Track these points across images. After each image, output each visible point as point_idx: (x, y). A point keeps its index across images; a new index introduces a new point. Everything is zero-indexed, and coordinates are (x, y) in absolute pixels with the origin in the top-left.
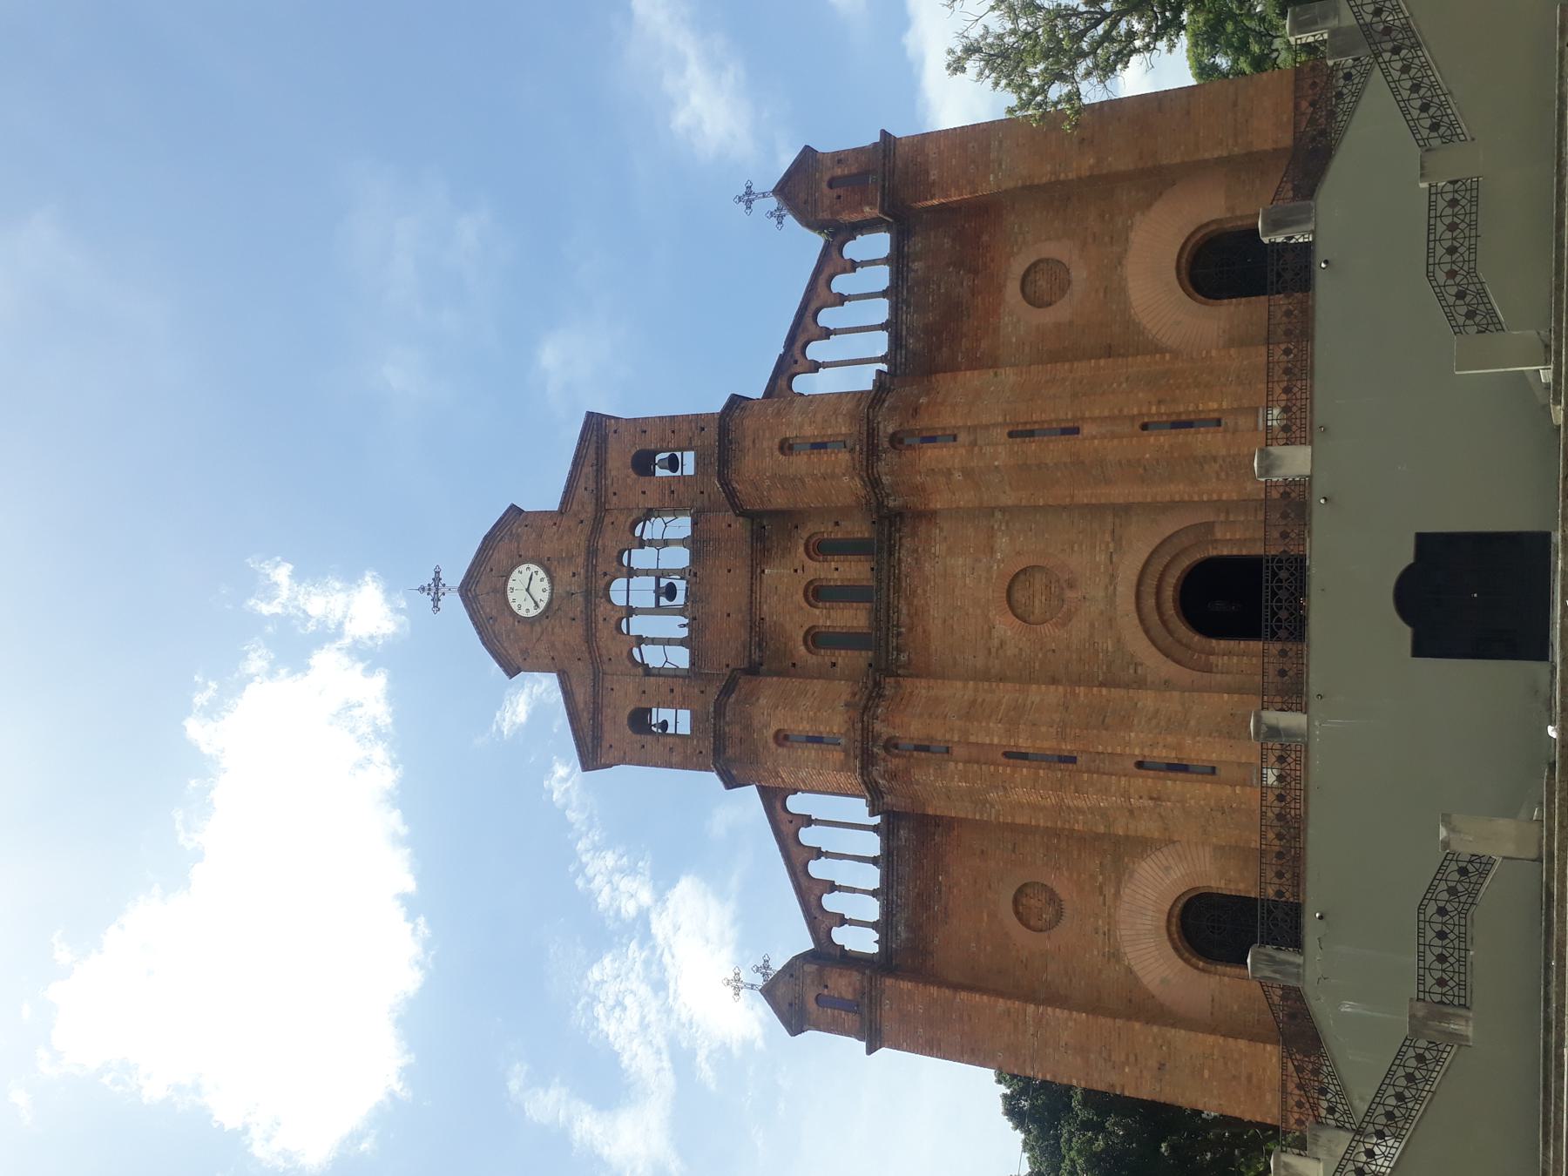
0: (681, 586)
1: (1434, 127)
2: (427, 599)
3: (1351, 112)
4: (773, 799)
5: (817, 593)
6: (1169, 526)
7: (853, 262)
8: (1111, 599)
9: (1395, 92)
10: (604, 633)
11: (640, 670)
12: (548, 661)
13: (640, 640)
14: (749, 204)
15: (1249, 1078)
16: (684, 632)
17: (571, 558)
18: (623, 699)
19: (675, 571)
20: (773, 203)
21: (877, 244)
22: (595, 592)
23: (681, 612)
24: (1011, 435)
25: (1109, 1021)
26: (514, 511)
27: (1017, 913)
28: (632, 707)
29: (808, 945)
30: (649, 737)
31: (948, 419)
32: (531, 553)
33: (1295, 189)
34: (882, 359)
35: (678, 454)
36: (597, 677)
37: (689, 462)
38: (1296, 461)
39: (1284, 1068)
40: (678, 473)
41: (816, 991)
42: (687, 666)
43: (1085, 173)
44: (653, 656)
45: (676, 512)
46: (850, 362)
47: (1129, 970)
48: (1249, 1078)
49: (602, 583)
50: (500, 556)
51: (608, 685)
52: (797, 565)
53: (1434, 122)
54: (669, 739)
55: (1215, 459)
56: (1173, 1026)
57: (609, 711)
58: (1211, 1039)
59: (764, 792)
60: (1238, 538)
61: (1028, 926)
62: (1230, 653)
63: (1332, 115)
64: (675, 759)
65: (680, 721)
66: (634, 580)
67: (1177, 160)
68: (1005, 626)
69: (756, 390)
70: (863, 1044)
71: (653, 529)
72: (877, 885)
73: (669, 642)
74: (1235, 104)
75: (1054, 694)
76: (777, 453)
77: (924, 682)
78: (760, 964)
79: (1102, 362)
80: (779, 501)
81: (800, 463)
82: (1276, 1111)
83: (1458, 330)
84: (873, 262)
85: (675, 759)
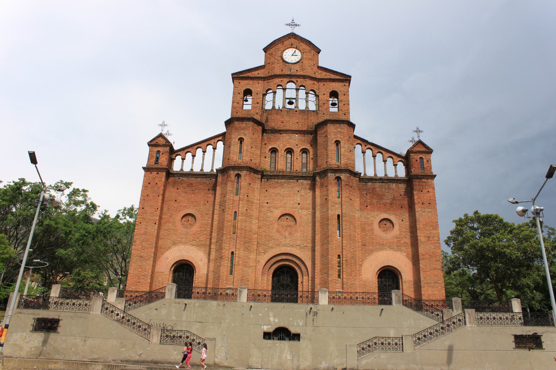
0: (292, 107)
1: (419, 339)
2: (290, 22)
3: (427, 316)
4: (223, 137)
6: (309, 264)
7: (397, 165)
8: (285, 245)
9: (430, 328)
10: (277, 81)
12: (268, 62)
13: (275, 93)
14: (416, 131)
15: (139, 282)
16: (277, 108)
17: (303, 70)
18: (257, 87)
19: (297, 104)
20: (417, 139)
21: (401, 172)
22: (291, 77)
23: (284, 107)
24: (338, 216)
25: (154, 242)
26: (318, 51)
28: (252, 90)
29: (176, 148)
30: (242, 96)
31: (345, 194)
32: (304, 56)
33: (406, 301)
34: (365, 174)
35: (337, 106)
37: (334, 110)
38: (323, 299)
39: (142, 292)
40: (330, 106)
41: (162, 149)
42: (266, 108)
43: (419, 238)
44: (269, 97)
45: (318, 105)
46: (368, 165)
47: (170, 248)
48: (139, 282)
49: (294, 80)
50: (303, 46)
51: (260, 81)
53: (421, 338)
54: (241, 102)
55: (328, 277)
58: (150, 271)
59: (224, 135)
60: (304, 283)
61: (183, 217)
62: (268, 280)
63: (427, 310)
64: (235, 104)
65: (248, 106)
66: (295, 91)
67: (421, 266)
68: (278, 213)
69: (357, 132)
70: (145, 166)
71: (312, 97)
72: (194, 171)
73: (274, 102)
74: (436, 283)
77: (259, 187)
78: (170, 133)
79: (360, 243)
80: (320, 140)
82: (130, 289)
83: (359, 345)
84: (396, 172)
85: (235, 104)
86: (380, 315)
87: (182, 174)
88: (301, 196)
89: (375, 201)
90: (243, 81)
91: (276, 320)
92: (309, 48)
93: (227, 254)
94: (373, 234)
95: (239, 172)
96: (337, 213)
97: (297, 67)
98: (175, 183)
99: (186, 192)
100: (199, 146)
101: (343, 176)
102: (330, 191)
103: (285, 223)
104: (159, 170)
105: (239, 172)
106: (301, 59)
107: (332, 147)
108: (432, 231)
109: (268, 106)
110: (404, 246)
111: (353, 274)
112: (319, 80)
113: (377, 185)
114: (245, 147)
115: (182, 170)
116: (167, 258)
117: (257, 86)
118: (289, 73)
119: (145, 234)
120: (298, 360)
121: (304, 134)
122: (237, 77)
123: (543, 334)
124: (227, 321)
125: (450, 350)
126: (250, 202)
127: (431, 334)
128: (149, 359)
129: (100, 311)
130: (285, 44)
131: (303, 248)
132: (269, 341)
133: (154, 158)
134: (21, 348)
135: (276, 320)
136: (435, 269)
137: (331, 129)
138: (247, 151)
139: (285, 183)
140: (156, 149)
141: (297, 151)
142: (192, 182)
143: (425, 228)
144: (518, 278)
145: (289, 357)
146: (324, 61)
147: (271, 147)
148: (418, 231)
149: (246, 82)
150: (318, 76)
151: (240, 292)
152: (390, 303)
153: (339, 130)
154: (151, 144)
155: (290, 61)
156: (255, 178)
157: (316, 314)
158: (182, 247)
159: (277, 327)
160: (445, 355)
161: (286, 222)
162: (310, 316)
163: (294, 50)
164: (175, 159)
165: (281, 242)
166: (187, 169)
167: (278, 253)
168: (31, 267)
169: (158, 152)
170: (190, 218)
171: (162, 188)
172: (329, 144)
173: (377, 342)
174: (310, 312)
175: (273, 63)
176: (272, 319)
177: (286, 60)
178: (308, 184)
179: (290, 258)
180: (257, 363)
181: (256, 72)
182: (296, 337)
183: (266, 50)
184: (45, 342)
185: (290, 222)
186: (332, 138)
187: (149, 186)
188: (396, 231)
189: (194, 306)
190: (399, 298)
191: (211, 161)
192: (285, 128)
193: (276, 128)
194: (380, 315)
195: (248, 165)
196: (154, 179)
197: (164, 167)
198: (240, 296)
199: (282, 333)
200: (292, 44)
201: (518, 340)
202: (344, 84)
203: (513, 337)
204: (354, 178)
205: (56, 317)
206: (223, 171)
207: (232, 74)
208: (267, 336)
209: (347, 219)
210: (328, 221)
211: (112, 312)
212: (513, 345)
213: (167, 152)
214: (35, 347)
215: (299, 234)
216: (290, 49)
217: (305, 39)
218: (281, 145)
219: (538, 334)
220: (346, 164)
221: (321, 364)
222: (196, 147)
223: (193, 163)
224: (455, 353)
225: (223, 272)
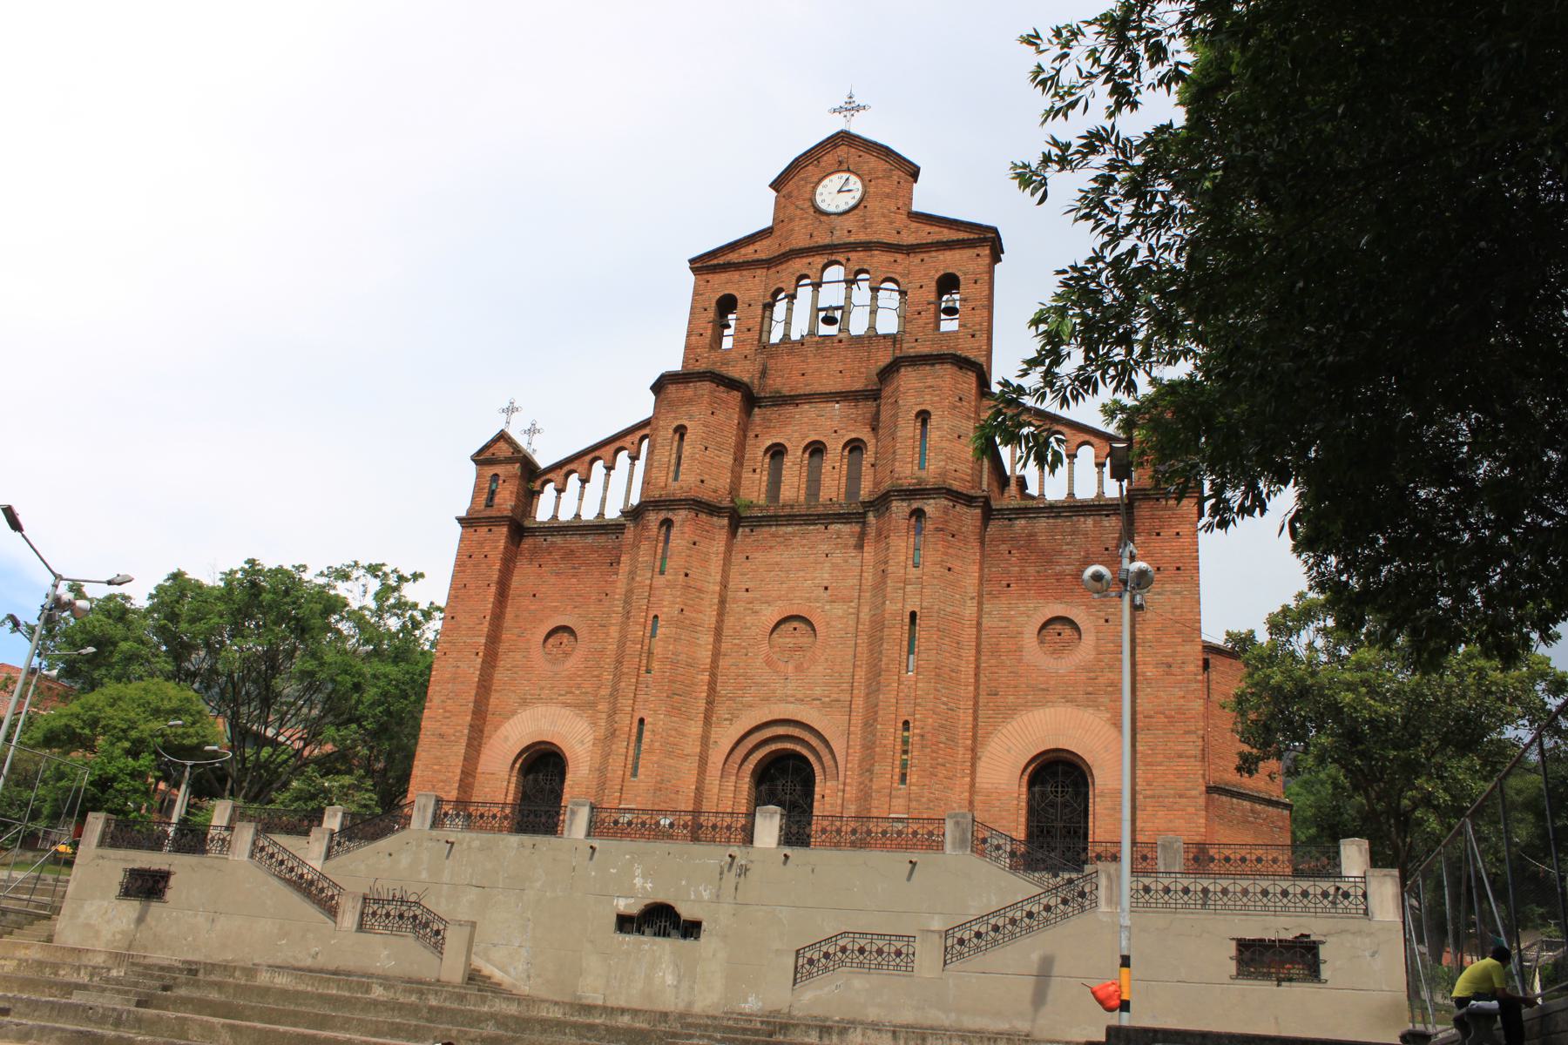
2: (841, 101)
10: (798, 265)
11: (769, 300)
22: (831, 252)
26: (914, 172)
29: (543, 461)
36: (769, 263)
41: (509, 471)
45: (903, 318)
47: (514, 713)
50: (872, 162)
56: (468, 745)
68: (771, 614)
70: (463, 514)
71: (889, 298)
75: (705, 656)
76: (919, 408)
86: (909, 879)
87: (556, 528)
88: (834, 566)
89: (1031, 570)
90: (717, 276)
91: (649, 885)
92: (887, 166)
93: (625, 722)
94: (1020, 661)
95: (670, 515)
96: (909, 609)
97: (850, 222)
98: (535, 552)
99: (558, 574)
100: (597, 454)
101: (931, 507)
102: (893, 549)
103: (789, 641)
104: (492, 522)
105: (670, 515)
106: (861, 200)
107: (908, 429)
108: (1180, 649)
109: (776, 336)
110: (1106, 692)
111: (942, 772)
112: (910, 250)
113: (1042, 524)
114: (687, 449)
115: (1071, 495)
116: (506, 738)
117: (751, 286)
118: (827, 241)
119: (454, 679)
120: (692, 988)
121: (857, 400)
122: (704, 265)
123: (1329, 939)
124: (538, 884)
125: (1044, 973)
126: (690, 587)
127: (996, 929)
128: (332, 967)
129: (247, 853)
131: (828, 705)
132: (628, 938)
133: (486, 492)
134: (97, 934)
135: (649, 885)
136: (1180, 756)
137: (908, 379)
138: (692, 458)
139: (794, 534)
140: (490, 471)
141: (835, 447)
142: (573, 547)
143: (1159, 641)
145: (670, 979)
146: (925, 198)
147: (769, 443)
149: (724, 276)
150: (908, 239)
151: (573, 813)
152: (940, 846)
153: (930, 381)
154: (483, 458)
155: (832, 209)
156: (713, 526)
157: (744, 870)
158: (540, 709)
159: (648, 901)
160: (1026, 987)
161: (786, 638)
162: (731, 877)
163: (845, 175)
164: (541, 492)
165: (774, 691)
166: (566, 515)
167: (765, 720)
168: (189, 763)
170: (565, 637)
172: (901, 422)
173: (849, 946)
174: (731, 865)
175: (791, 220)
176: (638, 881)
177: (824, 207)
178: (852, 534)
179: (796, 732)
180: (595, 991)
181: (750, 249)
182: (691, 929)
183: (776, 185)
184: (140, 920)
185: (801, 637)
187: (470, 563)
188: (1085, 650)
189: (469, 847)
190: (964, 832)
191: (610, 493)
192: (807, 390)
193: (786, 391)
194: (909, 879)
195: (692, 494)
196: (481, 544)
197: (505, 513)
198: (571, 821)
199: (659, 919)
200: (840, 163)
201: (1247, 954)
202: (976, 251)
203: (1234, 943)
204: (965, 509)
205: (165, 867)
206: (634, 514)
207: (692, 261)
208: (625, 923)
209: (934, 623)
210: (881, 631)
211: (272, 856)
212: (1232, 967)
213: (515, 476)
214: (123, 933)
215: (820, 668)
216: (835, 177)
217: (875, 144)
218: (796, 435)
219: (1313, 938)
220: (943, 474)
221: (746, 1001)
222: (588, 458)
223: (581, 498)
224: (1055, 984)
225: (614, 771)
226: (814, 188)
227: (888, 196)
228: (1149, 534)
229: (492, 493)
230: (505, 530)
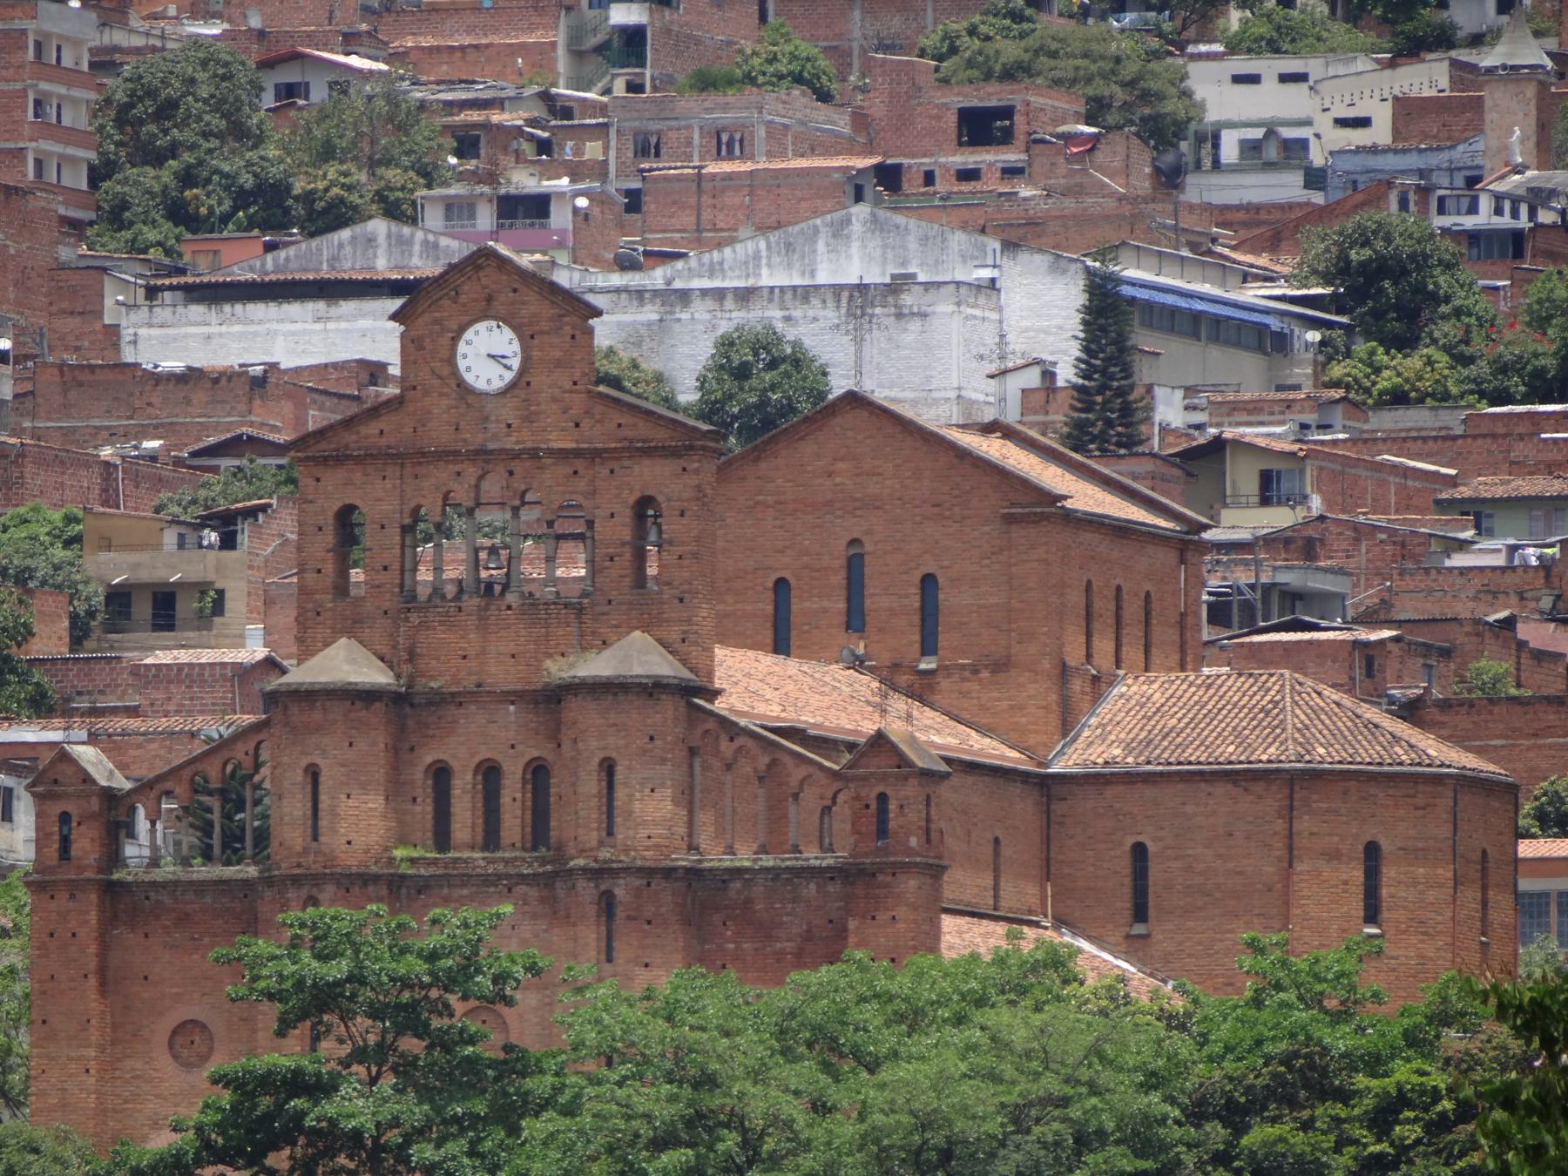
5: (490, 773)
27: (185, 1023)
50: (534, 305)
51: (389, 471)
52: (520, 747)
57: (358, 476)
61: (175, 1032)
81: (591, 785)
105: (314, 892)
130: (463, 299)
140: (56, 809)
144: (1141, 442)
147: (429, 759)
148: (793, 634)
163: (516, 363)
169: (65, 818)
171: (93, 949)
186: (593, 750)
200: (489, 299)
226: (455, 340)
227: (558, 364)
228: (864, 917)
229: (65, 843)
230: (94, 897)
